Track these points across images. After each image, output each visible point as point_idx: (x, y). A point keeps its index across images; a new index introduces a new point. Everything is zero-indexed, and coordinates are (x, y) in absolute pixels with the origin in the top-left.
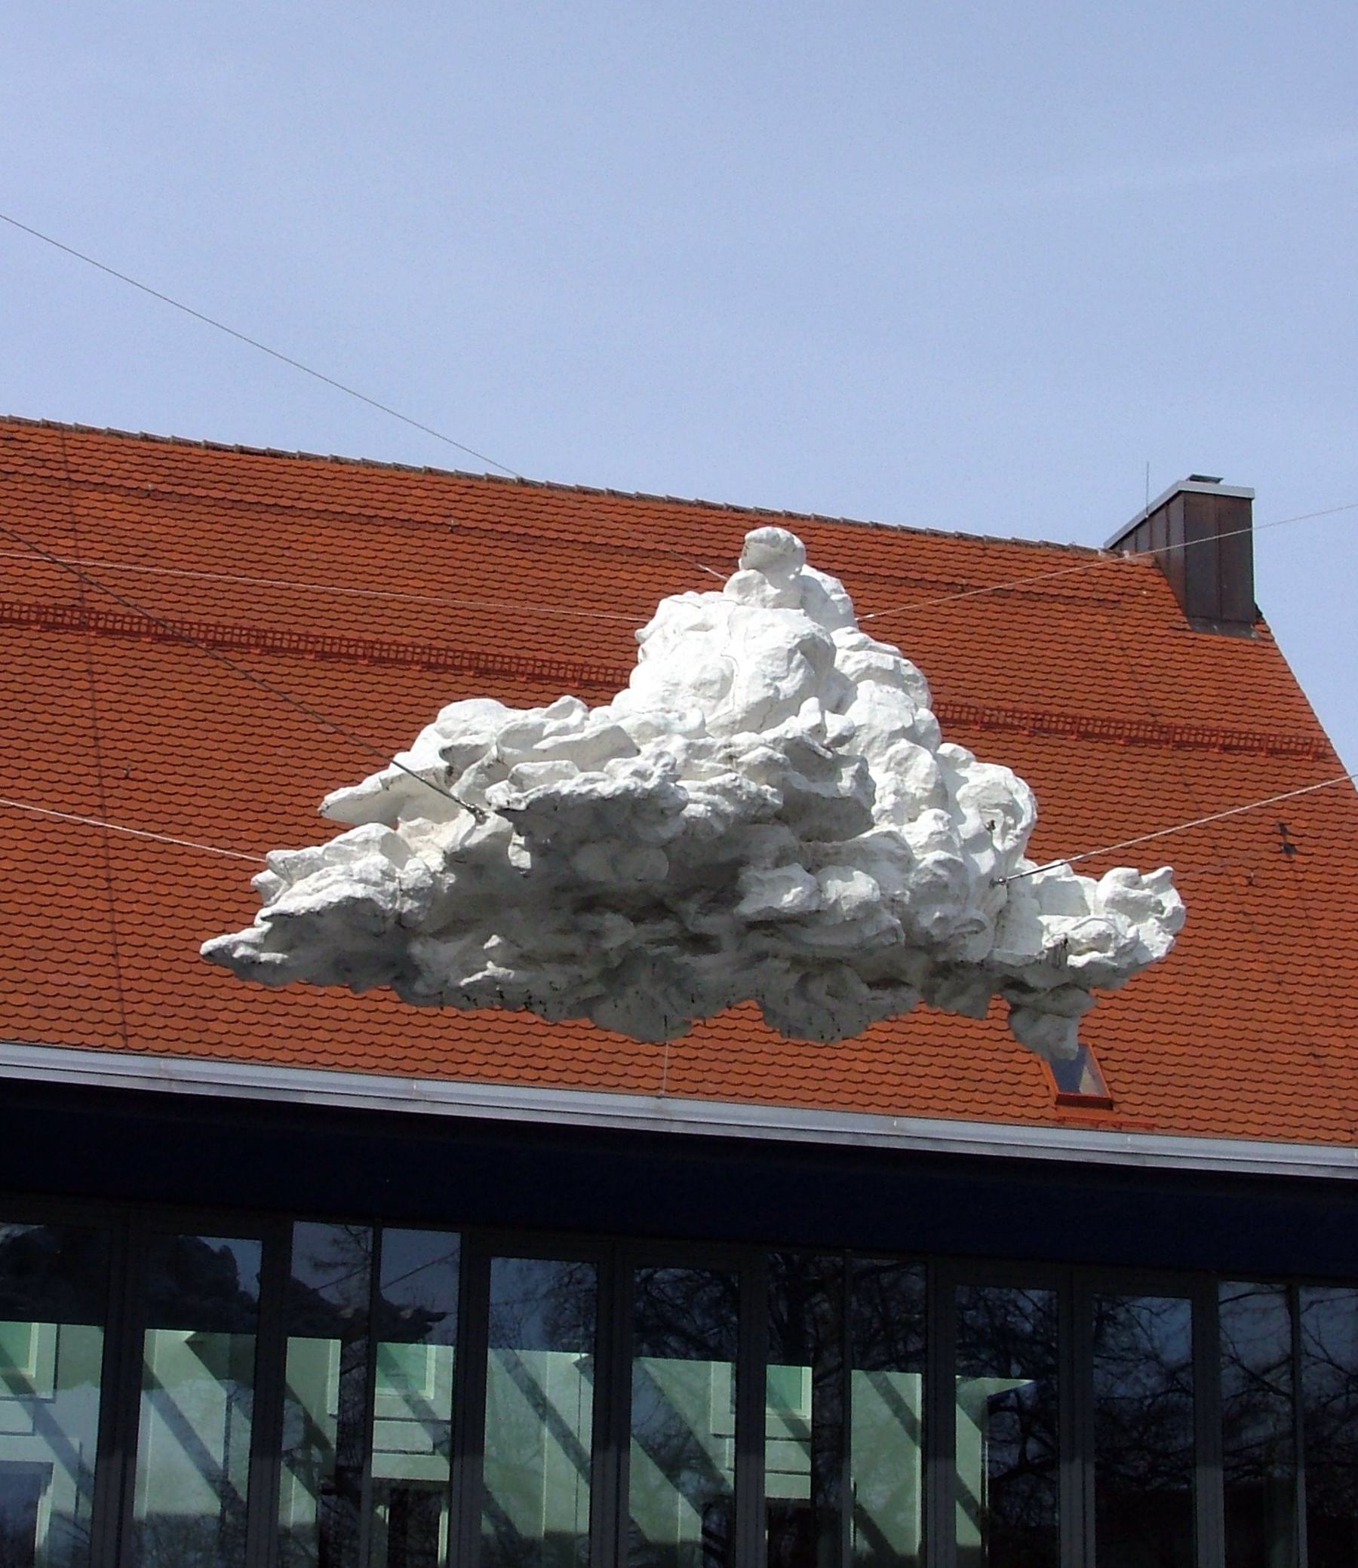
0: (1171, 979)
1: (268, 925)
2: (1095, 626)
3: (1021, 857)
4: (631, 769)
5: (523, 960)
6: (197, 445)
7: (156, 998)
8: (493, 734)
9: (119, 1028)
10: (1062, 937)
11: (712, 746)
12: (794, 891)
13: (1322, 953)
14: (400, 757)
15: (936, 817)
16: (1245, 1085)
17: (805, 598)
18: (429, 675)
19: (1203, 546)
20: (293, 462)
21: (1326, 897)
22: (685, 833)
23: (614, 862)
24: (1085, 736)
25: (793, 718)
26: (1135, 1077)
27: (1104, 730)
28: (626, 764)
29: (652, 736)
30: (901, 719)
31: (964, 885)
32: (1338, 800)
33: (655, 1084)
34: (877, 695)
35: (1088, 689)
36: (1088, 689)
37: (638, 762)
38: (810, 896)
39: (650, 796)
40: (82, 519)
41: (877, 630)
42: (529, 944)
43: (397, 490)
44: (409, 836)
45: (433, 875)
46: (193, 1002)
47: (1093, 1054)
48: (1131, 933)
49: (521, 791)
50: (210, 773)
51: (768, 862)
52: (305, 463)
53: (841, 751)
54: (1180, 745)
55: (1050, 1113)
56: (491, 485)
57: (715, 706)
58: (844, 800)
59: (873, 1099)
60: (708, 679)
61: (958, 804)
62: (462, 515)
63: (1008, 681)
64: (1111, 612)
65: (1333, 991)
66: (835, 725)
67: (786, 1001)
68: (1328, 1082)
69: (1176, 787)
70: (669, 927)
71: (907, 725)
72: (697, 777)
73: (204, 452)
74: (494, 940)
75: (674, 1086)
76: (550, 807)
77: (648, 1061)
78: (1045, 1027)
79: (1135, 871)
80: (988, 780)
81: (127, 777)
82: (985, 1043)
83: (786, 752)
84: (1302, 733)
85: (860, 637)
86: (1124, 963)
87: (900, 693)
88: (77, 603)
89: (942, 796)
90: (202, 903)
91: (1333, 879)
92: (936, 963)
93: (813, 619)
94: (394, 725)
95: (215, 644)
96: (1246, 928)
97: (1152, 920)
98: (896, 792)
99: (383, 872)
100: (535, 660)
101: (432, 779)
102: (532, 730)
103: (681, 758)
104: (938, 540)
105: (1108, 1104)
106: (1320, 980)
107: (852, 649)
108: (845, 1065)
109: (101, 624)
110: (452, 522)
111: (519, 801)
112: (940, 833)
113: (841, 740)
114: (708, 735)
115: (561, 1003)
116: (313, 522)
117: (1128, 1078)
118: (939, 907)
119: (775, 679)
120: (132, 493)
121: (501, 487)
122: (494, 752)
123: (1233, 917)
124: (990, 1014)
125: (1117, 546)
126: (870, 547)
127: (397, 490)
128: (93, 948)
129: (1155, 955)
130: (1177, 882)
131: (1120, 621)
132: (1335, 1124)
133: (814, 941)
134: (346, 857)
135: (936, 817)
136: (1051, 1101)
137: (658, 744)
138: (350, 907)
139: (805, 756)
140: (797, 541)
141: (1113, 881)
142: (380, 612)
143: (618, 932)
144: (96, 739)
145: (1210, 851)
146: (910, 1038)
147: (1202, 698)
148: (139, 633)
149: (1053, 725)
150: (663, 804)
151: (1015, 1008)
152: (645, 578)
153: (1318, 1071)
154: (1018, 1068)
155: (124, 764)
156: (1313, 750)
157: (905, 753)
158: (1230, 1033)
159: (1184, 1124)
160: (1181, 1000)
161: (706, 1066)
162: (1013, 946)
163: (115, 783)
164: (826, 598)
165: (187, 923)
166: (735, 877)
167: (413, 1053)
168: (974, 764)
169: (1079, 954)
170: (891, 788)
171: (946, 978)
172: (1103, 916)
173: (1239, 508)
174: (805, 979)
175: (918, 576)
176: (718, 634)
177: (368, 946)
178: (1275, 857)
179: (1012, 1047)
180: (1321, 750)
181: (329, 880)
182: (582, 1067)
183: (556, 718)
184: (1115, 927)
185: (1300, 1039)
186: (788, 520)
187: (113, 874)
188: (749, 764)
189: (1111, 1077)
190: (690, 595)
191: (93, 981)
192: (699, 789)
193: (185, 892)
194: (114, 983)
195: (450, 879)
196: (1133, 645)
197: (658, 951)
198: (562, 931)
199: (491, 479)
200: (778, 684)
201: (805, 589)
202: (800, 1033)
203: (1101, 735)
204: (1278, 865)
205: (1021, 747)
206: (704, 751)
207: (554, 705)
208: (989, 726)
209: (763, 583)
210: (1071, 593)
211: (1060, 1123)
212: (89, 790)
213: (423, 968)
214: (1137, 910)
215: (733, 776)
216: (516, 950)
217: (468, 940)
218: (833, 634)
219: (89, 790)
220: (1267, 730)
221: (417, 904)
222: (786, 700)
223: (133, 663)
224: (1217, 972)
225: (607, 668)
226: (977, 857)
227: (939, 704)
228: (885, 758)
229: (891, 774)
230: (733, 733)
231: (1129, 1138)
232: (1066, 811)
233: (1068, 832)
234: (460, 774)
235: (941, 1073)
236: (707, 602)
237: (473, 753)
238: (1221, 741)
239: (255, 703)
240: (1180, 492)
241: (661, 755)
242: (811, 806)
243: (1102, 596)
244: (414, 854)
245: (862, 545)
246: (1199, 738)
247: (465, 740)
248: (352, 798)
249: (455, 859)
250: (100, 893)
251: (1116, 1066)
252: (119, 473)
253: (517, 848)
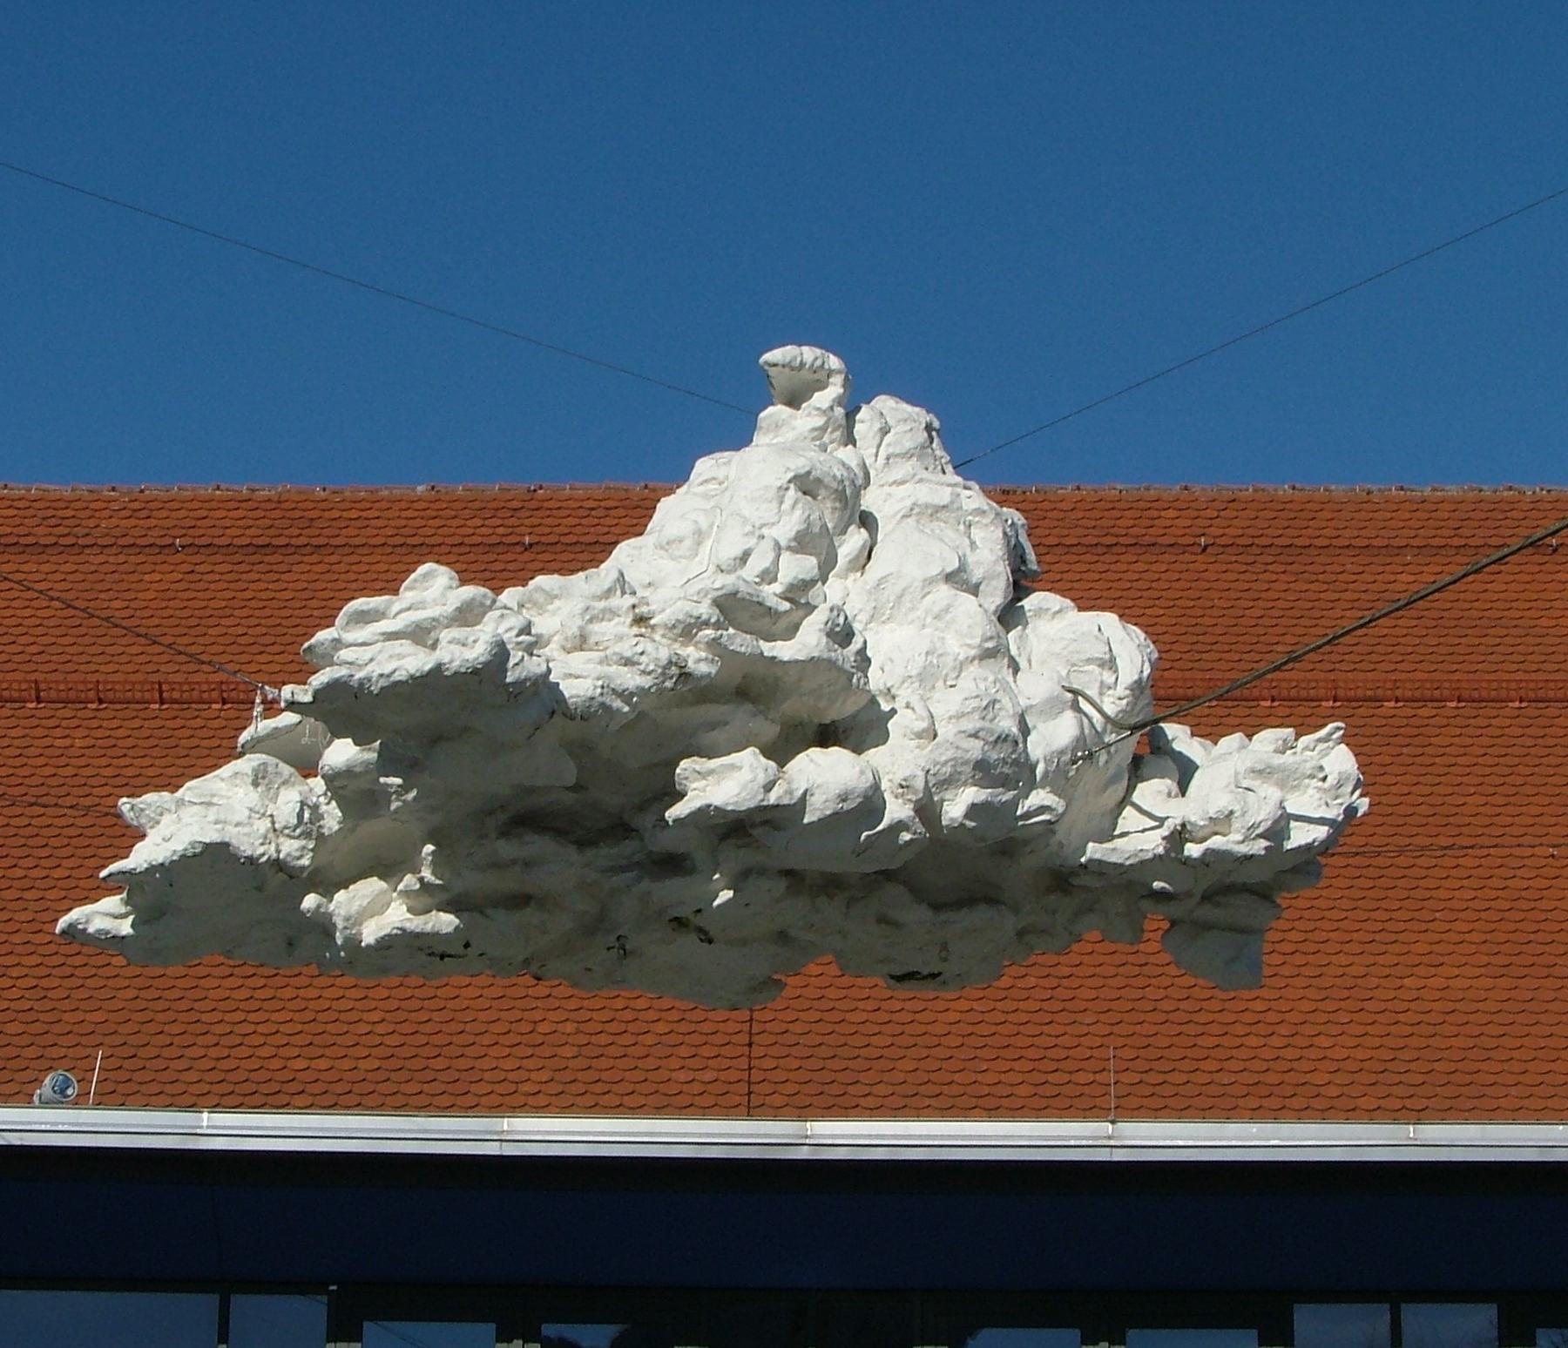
10: (1178, 821)
70: (629, 847)
97: (1311, 791)
157: (945, 603)
207: (413, 576)
233: (1203, 687)
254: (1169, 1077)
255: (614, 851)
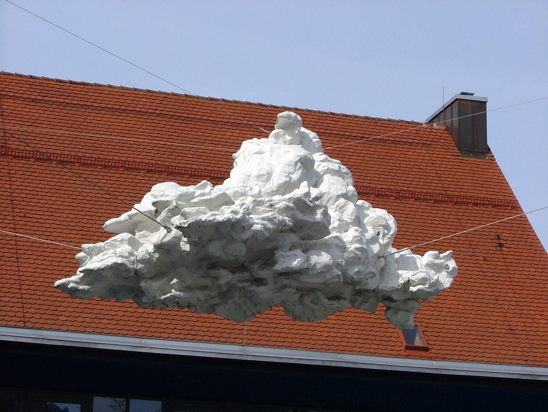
0: (452, 298)
1: (82, 274)
2: (421, 154)
3: (391, 247)
4: (231, 210)
5: (187, 289)
6: (52, 80)
7: (37, 306)
8: (174, 196)
9: (22, 319)
11: (264, 201)
12: (297, 260)
13: (515, 288)
14: (136, 206)
15: (356, 230)
16: (483, 342)
17: (302, 141)
18: (148, 175)
19: (466, 121)
20: (92, 87)
21: (516, 265)
22: (252, 236)
23: (223, 248)
24: (417, 199)
25: (297, 189)
26: (437, 338)
27: (425, 197)
28: (228, 208)
29: (239, 197)
30: (341, 190)
31: (367, 258)
32: (521, 225)
33: (241, 341)
34: (331, 180)
35: (418, 180)
36: (418, 180)
37: (233, 207)
38: (304, 262)
39: (238, 221)
40: (6, 111)
41: (331, 154)
42: (189, 282)
43: (135, 99)
44: (140, 238)
45: (150, 254)
46: (52, 308)
47: (420, 329)
48: (435, 277)
49: (186, 219)
50: (59, 215)
51: (287, 248)
52: (97, 88)
53: (317, 203)
54: (456, 203)
55: (403, 353)
56: (174, 97)
57: (265, 185)
58: (318, 223)
59: (330, 347)
60: (262, 174)
61: (364, 225)
62: (162, 109)
63: (386, 177)
64: (428, 149)
65: (519, 303)
66: (314, 192)
67: (294, 305)
68: (516, 341)
69: (455, 220)
70: (246, 275)
71: (344, 193)
72: (257, 213)
73: (55, 83)
74: (175, 281)
75: (249, 342)
76: (197, 226)
77: (238, 332)
78: (400, 316)
79: (437, 252)
80: (378, 215)
81: (25, 216)
82: (376, 325)
83: (294, 203)
84: (507, 198)
85: (324, 156)
86: (432, 290)
87: (341, 179)
88: (3, 145)
89: (358, 221)
90: (56, 268)
91: (519, 258)
92: (355, 290)
93: (305, 149)
94: (134, 195)
95: (61, 162)
96: (483, 278)
97: (444, 272)
98: (339, 220)
99: (129, 253)
100: (192, 169)
101: (149, 215)
102: (190, 194)
103: (251, 206)
104: (357, 119)
105: (426, 349)
106: (514, 299)
107: (320, 161)
108: (319, 334)
109: (14, 153)
110: (158, 112)
111: (185, 223)
112: (357, 236)
113: (317, 198)
114: (262, 196)
115: (203, 306)
116: (101, 112)
117: (435, 339)
118: (357, 267)
119: (289, 174)
120: (26, 100)
121: (178, 98)
122: (174, 203)
123: (478, 273)
124: (377, 313)
125: (431, 121)
126: (329, 122)
127: (135, 99)
128: (11, 286)
129: (445, 287)
130: (455, 256)
131: (432, 152)
132: (520, 358)
133: (304, 280)
134: (114, 246)
135: (356, 230)
136: (403, 348)
137: (241, 200)
138: (115, 267)
139: (302, 205)
140: (299, 117)
141: (428, 256)
142: (128, 149)
143: (225, 277)
144: (12, 201)
145: (468, 246)
146: (346, 322)
147: (465, 184)
148: (29, 158)
149: (404, 195)
150: (243, 224)
151: (388, 308)
152: (237, 135)
153: (513, 336)
154: (390, 335)
155: (23, 211)
156: (511, 205)
157: (343, 204)
158: (476, 320)
159: (457, 357)
160: (457, 307)
161: (262, 334)
162: (387, 283)
163: (20, 219)
164: (311, 141)
165: (49, 276)
166: (273, 255)
167: (142, 329)
168: (371, 208)
169: (414, 286)
170: (338, 218)
171: (360, 296)
172: (424, 270)
173: (481, 105)
174: (301, 297)
175: (349, 134)
176: (267, 155)
177: (123, 283)
178: (495, 249)
179: (387, 326)
180: (514, 205)
181: (107, 256)
182: (212, 334)
183: (200, 190)
184: (429, 275)
185: (505, 323)
186: (296, 110)
187: (19, 256)
188: (279, 209)
189: (427, 338)
190: (255, 139)
191: (11, 300)
192: (259, 219)
193: (49, 263)
194: (20, 300)
195: (157, 255)
196: (437, 162)
197: (242, 285)
198: (202, 277)
199: (174, 94)
200: (291, 176)
201: (302, 137)
202: (300, 319)
203: (424, 199)
204: (496, 252)
205: (391, 204)
206: (261, 203)
207: (199, 184)
208: (378, 195)
209: (285, 135)
210: (412, 141)
211: (407, 356)
212: (9, 222)
213: (146, 292)
214: (438, 268)
215: (272, 213)
216: (184, 284)
217: (164, 280)
218: (314, 156)
219: (9, 222)
220: (493, 197)
221: (143, 266)
222: (294, 182)
223: (27, 170)
224: (471, 296)
225: (221, 172)
226: (372, 247)
227: (358, 186)
228: (335, 206)
229: (337, 213)
230: (272, 195)
231: (435, 363)
232: (409, 230)
234: (161, 213)
235: (358, 336)
236: (262, 142)
237: (166, 204)
238: (473, 202)
239: (77, 186)
240: (457, 99)
241: (243, 204)
242: (304, 225)
243: (424, 142)
244: (142, 245)
245: (326, 121)
246: (464, 200)
247: (162, 199)
248: (116, 223)
249: (159, 247)
250: (14, 264)
251: (430, 334)
252: (20, 92)
253: (184, 243)
254: (34, 283)
255: (241, 275)
